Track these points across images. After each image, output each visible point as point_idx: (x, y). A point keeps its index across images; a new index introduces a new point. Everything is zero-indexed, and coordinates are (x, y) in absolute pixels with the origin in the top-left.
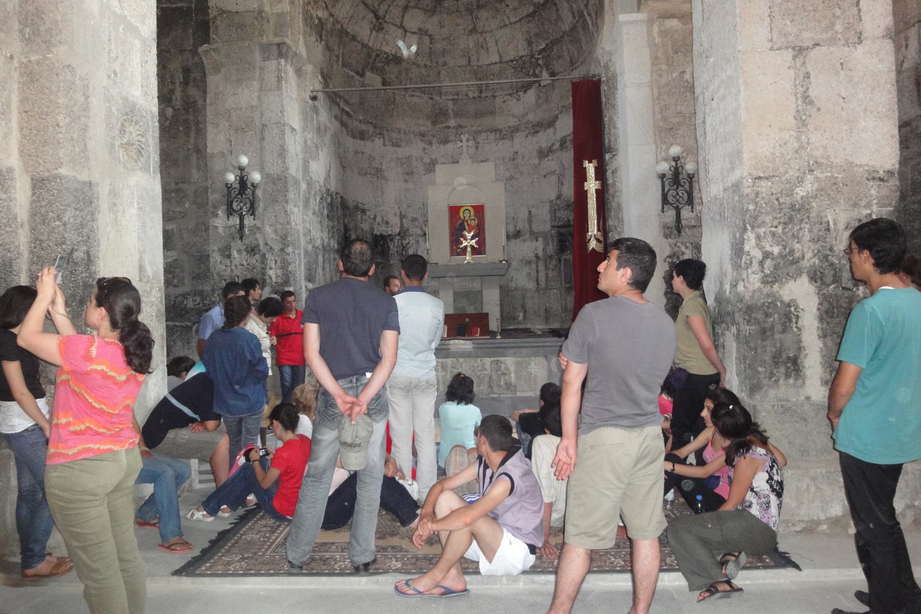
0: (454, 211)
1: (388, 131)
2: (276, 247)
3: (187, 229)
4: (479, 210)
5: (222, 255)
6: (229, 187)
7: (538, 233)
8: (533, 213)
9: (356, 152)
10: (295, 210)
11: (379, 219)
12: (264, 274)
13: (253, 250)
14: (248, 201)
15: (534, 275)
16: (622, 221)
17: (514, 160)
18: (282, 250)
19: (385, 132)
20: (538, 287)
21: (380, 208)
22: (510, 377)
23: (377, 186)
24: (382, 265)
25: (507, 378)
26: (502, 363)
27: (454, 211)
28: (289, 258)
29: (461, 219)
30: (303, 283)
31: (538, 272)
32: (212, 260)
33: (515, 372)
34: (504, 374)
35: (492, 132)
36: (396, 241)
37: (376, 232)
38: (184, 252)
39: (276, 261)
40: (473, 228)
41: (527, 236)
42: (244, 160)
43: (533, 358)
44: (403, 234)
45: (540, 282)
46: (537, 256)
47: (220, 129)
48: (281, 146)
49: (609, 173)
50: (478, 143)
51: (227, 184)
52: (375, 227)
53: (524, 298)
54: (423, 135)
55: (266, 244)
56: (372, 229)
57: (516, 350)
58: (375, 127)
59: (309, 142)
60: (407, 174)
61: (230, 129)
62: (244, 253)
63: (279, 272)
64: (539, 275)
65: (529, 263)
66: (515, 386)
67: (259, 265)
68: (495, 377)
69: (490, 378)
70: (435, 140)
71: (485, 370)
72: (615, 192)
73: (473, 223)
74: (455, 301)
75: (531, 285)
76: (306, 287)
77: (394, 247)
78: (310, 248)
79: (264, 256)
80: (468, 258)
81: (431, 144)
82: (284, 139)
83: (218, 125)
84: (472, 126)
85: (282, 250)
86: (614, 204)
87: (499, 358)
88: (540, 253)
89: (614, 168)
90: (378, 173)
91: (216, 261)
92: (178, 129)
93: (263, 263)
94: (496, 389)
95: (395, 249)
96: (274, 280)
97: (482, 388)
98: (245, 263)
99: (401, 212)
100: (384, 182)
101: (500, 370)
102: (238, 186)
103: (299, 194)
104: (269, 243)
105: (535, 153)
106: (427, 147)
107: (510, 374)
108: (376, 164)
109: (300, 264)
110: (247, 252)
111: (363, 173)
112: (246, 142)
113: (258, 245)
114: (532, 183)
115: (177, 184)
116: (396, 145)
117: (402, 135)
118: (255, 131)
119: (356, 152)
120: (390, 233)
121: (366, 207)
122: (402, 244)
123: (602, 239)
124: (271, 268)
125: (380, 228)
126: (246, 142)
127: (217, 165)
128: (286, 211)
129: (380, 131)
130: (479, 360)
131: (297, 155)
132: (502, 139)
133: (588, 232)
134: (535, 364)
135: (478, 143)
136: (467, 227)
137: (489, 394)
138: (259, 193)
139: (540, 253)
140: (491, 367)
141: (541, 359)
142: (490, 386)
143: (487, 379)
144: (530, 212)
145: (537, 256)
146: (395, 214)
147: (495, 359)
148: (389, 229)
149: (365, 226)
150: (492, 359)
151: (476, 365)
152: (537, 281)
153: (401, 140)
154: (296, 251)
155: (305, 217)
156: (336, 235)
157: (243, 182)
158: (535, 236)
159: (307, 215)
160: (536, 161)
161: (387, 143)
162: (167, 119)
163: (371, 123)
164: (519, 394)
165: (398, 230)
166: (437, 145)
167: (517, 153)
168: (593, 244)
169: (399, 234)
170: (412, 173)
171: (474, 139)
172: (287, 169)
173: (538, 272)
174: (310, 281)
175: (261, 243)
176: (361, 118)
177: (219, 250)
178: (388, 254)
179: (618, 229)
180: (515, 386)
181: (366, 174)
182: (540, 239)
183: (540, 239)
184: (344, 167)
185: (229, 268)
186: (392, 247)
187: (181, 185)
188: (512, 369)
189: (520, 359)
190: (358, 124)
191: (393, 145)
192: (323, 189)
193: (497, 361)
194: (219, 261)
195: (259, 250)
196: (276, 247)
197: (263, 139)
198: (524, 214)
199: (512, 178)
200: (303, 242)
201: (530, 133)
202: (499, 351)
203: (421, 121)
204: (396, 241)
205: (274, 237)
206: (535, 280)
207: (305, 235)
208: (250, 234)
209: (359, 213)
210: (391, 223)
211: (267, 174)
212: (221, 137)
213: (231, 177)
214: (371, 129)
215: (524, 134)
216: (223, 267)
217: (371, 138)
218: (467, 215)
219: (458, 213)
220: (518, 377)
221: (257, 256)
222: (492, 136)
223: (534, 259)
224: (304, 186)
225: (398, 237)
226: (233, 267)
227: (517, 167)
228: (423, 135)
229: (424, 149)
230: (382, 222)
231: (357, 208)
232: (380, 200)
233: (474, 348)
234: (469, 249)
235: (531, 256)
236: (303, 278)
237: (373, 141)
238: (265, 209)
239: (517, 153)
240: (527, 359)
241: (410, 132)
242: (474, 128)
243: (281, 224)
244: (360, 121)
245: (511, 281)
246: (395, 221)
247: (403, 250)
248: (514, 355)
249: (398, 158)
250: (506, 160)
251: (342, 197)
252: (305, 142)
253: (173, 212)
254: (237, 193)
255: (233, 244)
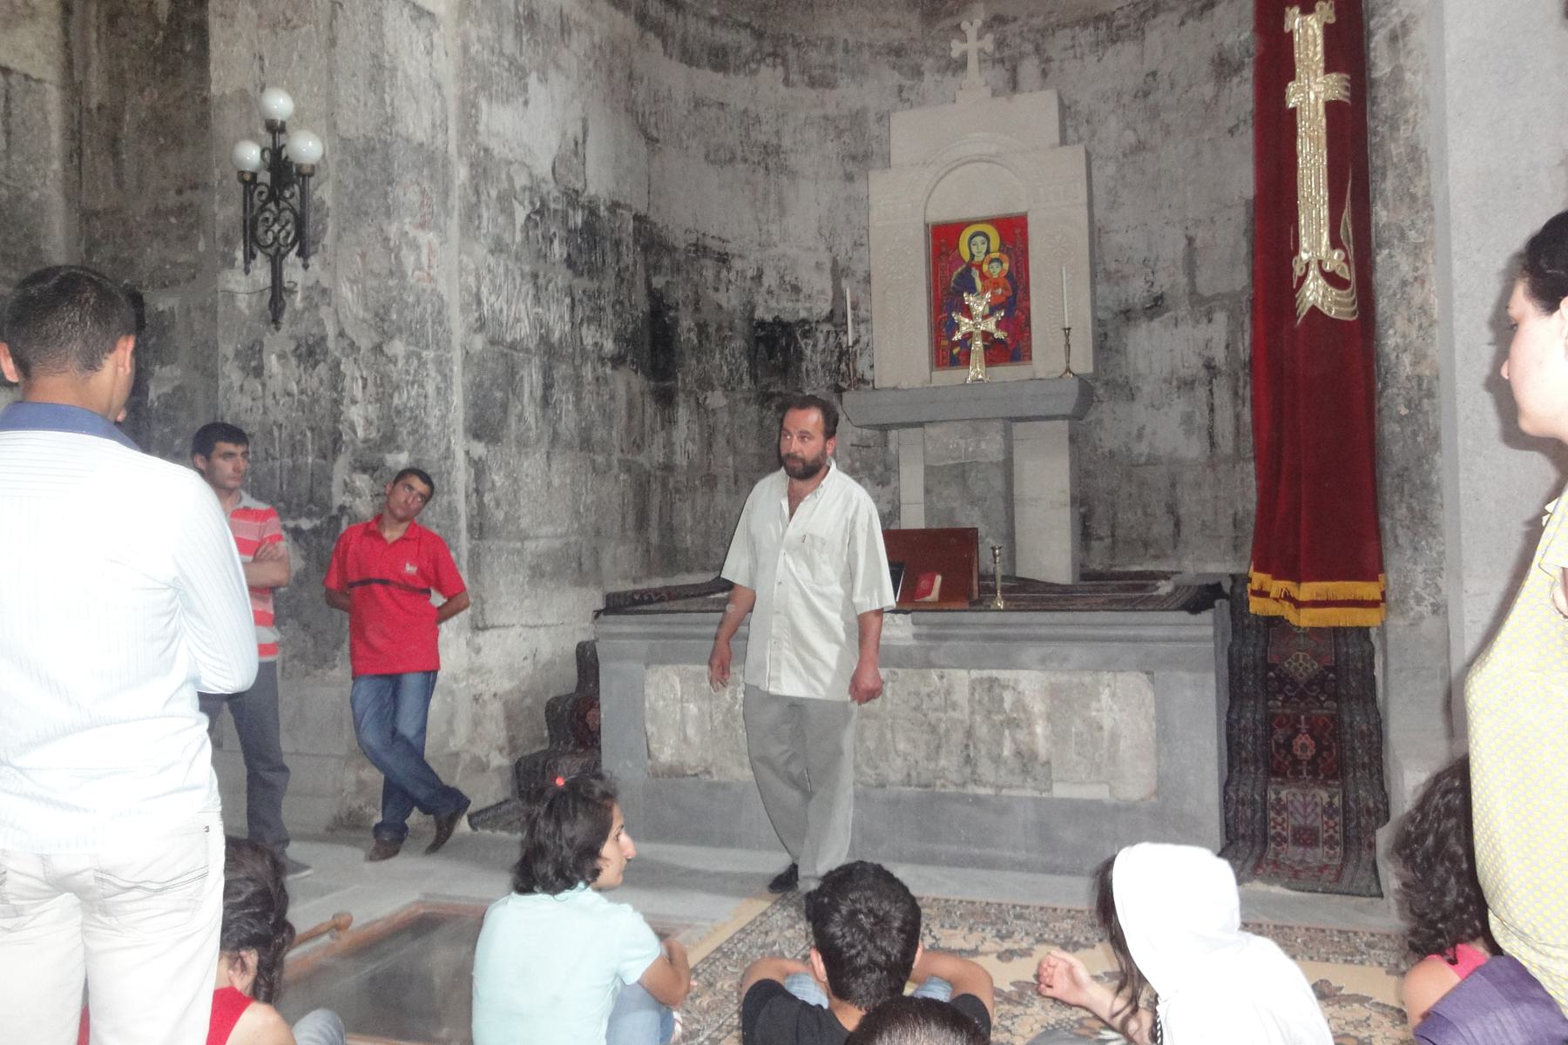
0: (944, 238)
1: (797, 45)
2: (365, 344)
3: (202, 309)
4: (1013, 230)
5: (243, 369)
6: (249, 182)
7: (1213, 298)
8: (1198, 243)
9: (698, 103)
10: (427, 238)
11: (770, 279)
12: (336, 417)
13: (311, 353)
14: (287, 215)
15: (1201, 418)
16: (1428, 205)
17: (1146, 94)
18: (378, 349)
19: (789, 49)
20: (1210, 457)
21: (773, 251)
22: (1032, 734)
23: (766, 195)
24: (779, 400)
25: (1021, 735)
26: (1005, 687)
27: (944, 238)
28: (395, 372)
29: (962, 260)
30: (460, 445)
31: (1212, 410)
32: (222, 383)
33: (1049, 718)
34: (1012, 723)
35: (1086, 26)
36: (821, 337)
37: (760, 313)
38: (196, 367)
39: (365, 380)
40: (996, 284)
41: (1183, 311)
42: (280, 104)
43: (1106, 677)
44: (835, 319)
45: (1219, 439)
46: (1210, 366)
47: (238, 28)
48: (375, 56)
49: (1378, 45)
50: (1049, 60)
51: (241, 173)
52: (759, 299)
53: (1173, 485)
54: (898, 52)
55: (342, 334)
56: (751, 307)
57: (1048, 648)
58: (759, 35)
59: (474, 48)
60: (854, 158)
61: (258, 26)
62: (293, 361)
63: (373, 411)
64: (1218, 418)
65: (1187, 385)
66: (1047, 763)
67: (326, 394)
68: (983, 731)
69: (969, 733)
70: (928, 63)
71: (954, 706)
72: (1402, 106)
73: (996, 271)
74: (927, 491)
75: (1194, 449)
76: (467, 453)
77: (814, 354)
78: (478, 342)
79: (337, 364)
80: (976, 370)
81: (917, 73)
82: (382, 36)
83: (233, 17)
84: (1031, 15)
85: (378, 349)
86: (1396, 150)
87: (994, 673)
88: (1220, 356)
89: (1397, 21)
90: (770, 157)
91: (231, 386)
92: (182, 51)
93: (334, 388)
94: (986, 769)
95: (818, 359)
96: (360, 433)
97: (943, 762)
98: (294, 388)
99: (835, 262)
100: (784, 180)
101: (1000, 710)
102: (265, 177)
103: (446, 193)
104: (348, 331)
105: (1205, 68)
106: (908, 83)
107: (1030, 725)
108: (763, 134)
109: (443, 393)
110: (299, 357)
111: (720, 158)
112: (295, 57)
113: (323, 339)
114: (1198, 154)
115: (180, 192)
116: (819, 81)
117: (839, 54)
118: (317, 26)
119: (698, 103)
120: (803, 314)
121: (731, 248)
122: (839, 345)
123: (1347, 274)
124: (354, 402)
125: (773, 304)
126: (295, 57)
127: (226, 120)
128: (387, 239)
129: (772, 46)
130: (934, 674)
131: (439, 87)
132: (1114, 42)
133: (1296, 252)
134: (1113, 695)
135: (1049, 60)
136: (979, 284)
137: (964, 784)
138: (324, 192)
139: (1220, 356)
140: (971, 701)
141: (1134, 681)
142: (968, 760)
143: (957, 737)
144: (1190, 241)
145: (1210, 366)
146: (818, 266)
147: (986, 673)
148: (799, 305)
149: (730, 299)
150: (975, 674)
151: (924, 690)
152: (1211, 436)
153: (833, 67)
154: (429, 354)
155: (465, 258)
156: (609, 315)
157: (281, 168)
158: (1203, 306)
159: (470, 254)
160: (1208, 90)
161: (794, 77)
162: (158, 25)
163: (747, 26)
164: (1060, 791)
165: (824, 308)
166: (938, 77)
167: (1154, 74)
168: (1314, 292)
169: (830, 318)
170: (867, 156)
171: (1037, 49)
172: (390, 120)
173: (1212, 410)
174: (477, 436)
175: (331, 331)
176: (715, 12)
177: (238, 354)
178: (799, 369)
179: (1412, 234)
180: (1047, 763)
181: (732, 159)
182: (1220, 317)
183: (1220, 317)
184: (651, 141)
185: (260, 403)
186: (808, 352)
187: (188, 195)
188: (1038, 707)
189: (1063, 678)
190: (702, 25)
191: (812, 83)
192: (551, 189)
193: (993, 682)
194: (237, 385)
195: (326, 353)
196: (365, 344)
197: (333, 42)
198: (1173, 247)
199: (1140, 147)
200: (458, 324)
201: (1190, 14)
202: (1004, 650)
203: (891, 16)
204: (821, 337)
205: (361, 313)
206: (1204, 433)
207: (464, 309)
208: (305, 309)
209: (709, 263)
210: (806, 291)
211: (342, 139)
212: (241, 50)
213: (251, 155)
214: (746, 41)
215: (1175, 18)
216: (246, 402)
217: (746, 65)
218: (979, 248)
219: (955, 246)
220: (1059, 737)
221: (322, 369)
222: (1086, 36)
223: (1203, 373)
224: (461, 173)
225: (826, 327)
226: (270, 401)
227: (1154, 113)
228: (898, 52)
229: (901, 89)
230: (780, 286)
231: (700, 250)
232: (774, 228)
233: (916, 636)
234: (978, 344)
235: (1192, 365)
236: (460, 428)
237: (754, 72)
238: (339, 238)
239: (1154, 74)
240: (1087, 679)
241: (860, 47)
242: (1037, 22)
243: (377, 276)
244: (713, 21)
245: (1140, 437)
246: (819, 284)
247: (840, 360)
248: (1043, 661)
249: (826, 118)
250: (1126, 99)
251: (637, 218)
252: (465, 49)
253: (174, 264)
254: (264, 197)
255: (267, 339)
